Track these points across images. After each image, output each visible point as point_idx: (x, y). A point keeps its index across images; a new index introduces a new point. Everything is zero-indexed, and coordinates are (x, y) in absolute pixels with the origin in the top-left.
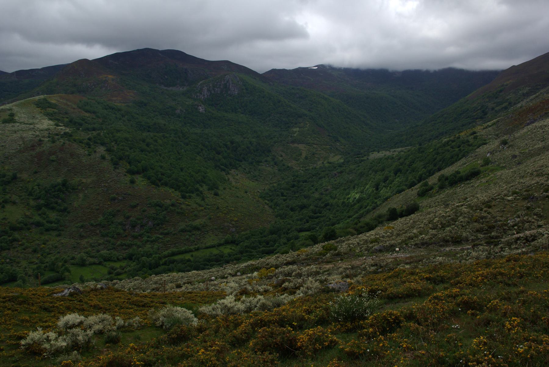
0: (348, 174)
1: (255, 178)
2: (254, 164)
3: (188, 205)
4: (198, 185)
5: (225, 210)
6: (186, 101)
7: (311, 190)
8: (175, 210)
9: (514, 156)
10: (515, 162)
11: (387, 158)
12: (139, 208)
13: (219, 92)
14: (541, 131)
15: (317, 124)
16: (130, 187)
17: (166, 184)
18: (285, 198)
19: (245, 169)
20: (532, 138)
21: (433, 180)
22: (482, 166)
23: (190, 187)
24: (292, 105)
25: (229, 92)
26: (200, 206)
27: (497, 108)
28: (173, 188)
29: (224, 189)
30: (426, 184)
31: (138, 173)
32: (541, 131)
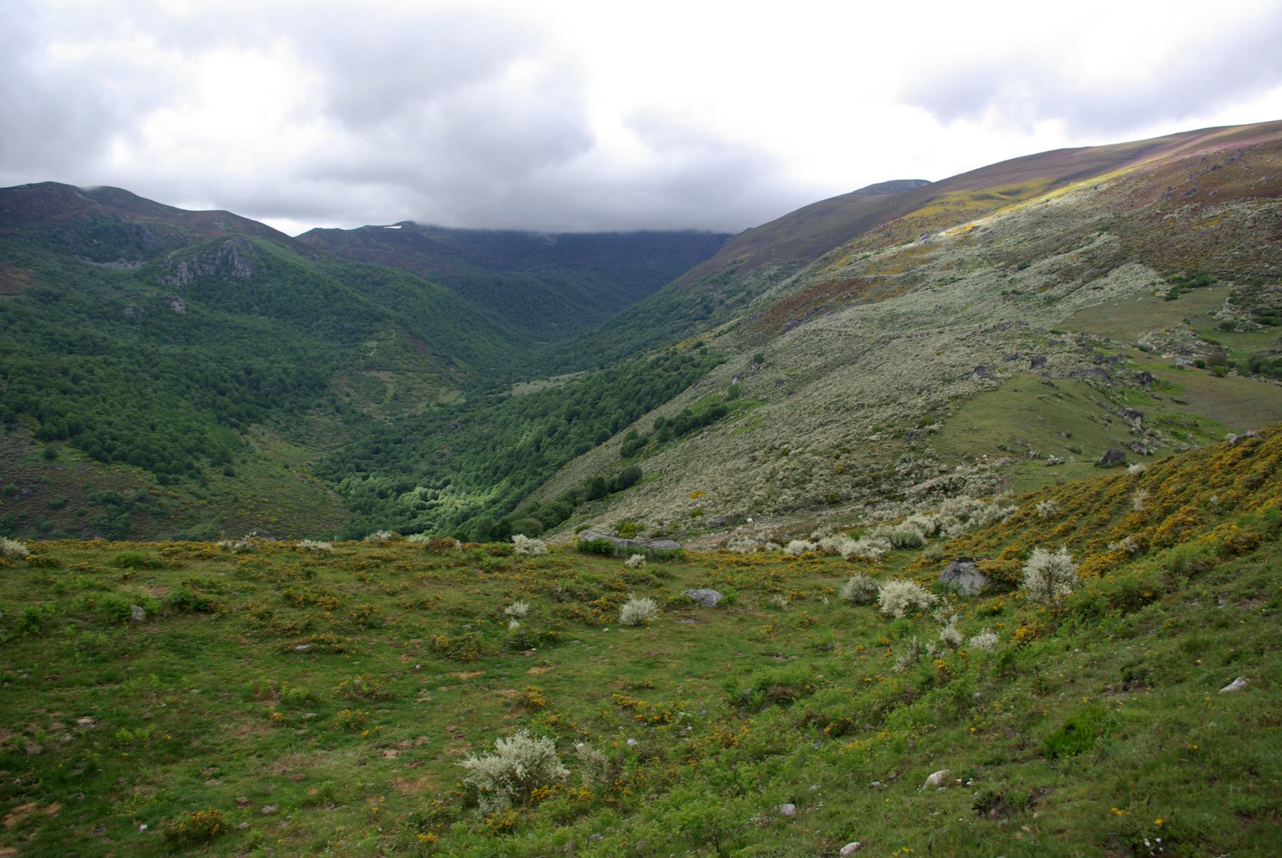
0: (479, 424)
1: (300, 440)
2: (296, 412)
3: (174, 497)
4: (190, 457)
5: (250, 503)
6: (145, 291)
7: (413, 456)
8: (147, 508)
9: (780, 382)
10: (782, 391)
11: (550, 393)
12: (69, 508)
13: (212, 273)
14: (817, 339)
15: (411, 333)
16: (45, 468)
17: (123, 458)
18: (364, 474)
19: (278, 423)
20: (803, 350)
21: (645, 425)
22: (728, 400)
23: (174, 462)
24: (360, 298)
25: (233, 274)
26: (199, 497)
27: (729, 302)
28: (138, 465)
29: (244, 462)
30: (633, 435)
31: (60, 437)
32: (817, 339)
